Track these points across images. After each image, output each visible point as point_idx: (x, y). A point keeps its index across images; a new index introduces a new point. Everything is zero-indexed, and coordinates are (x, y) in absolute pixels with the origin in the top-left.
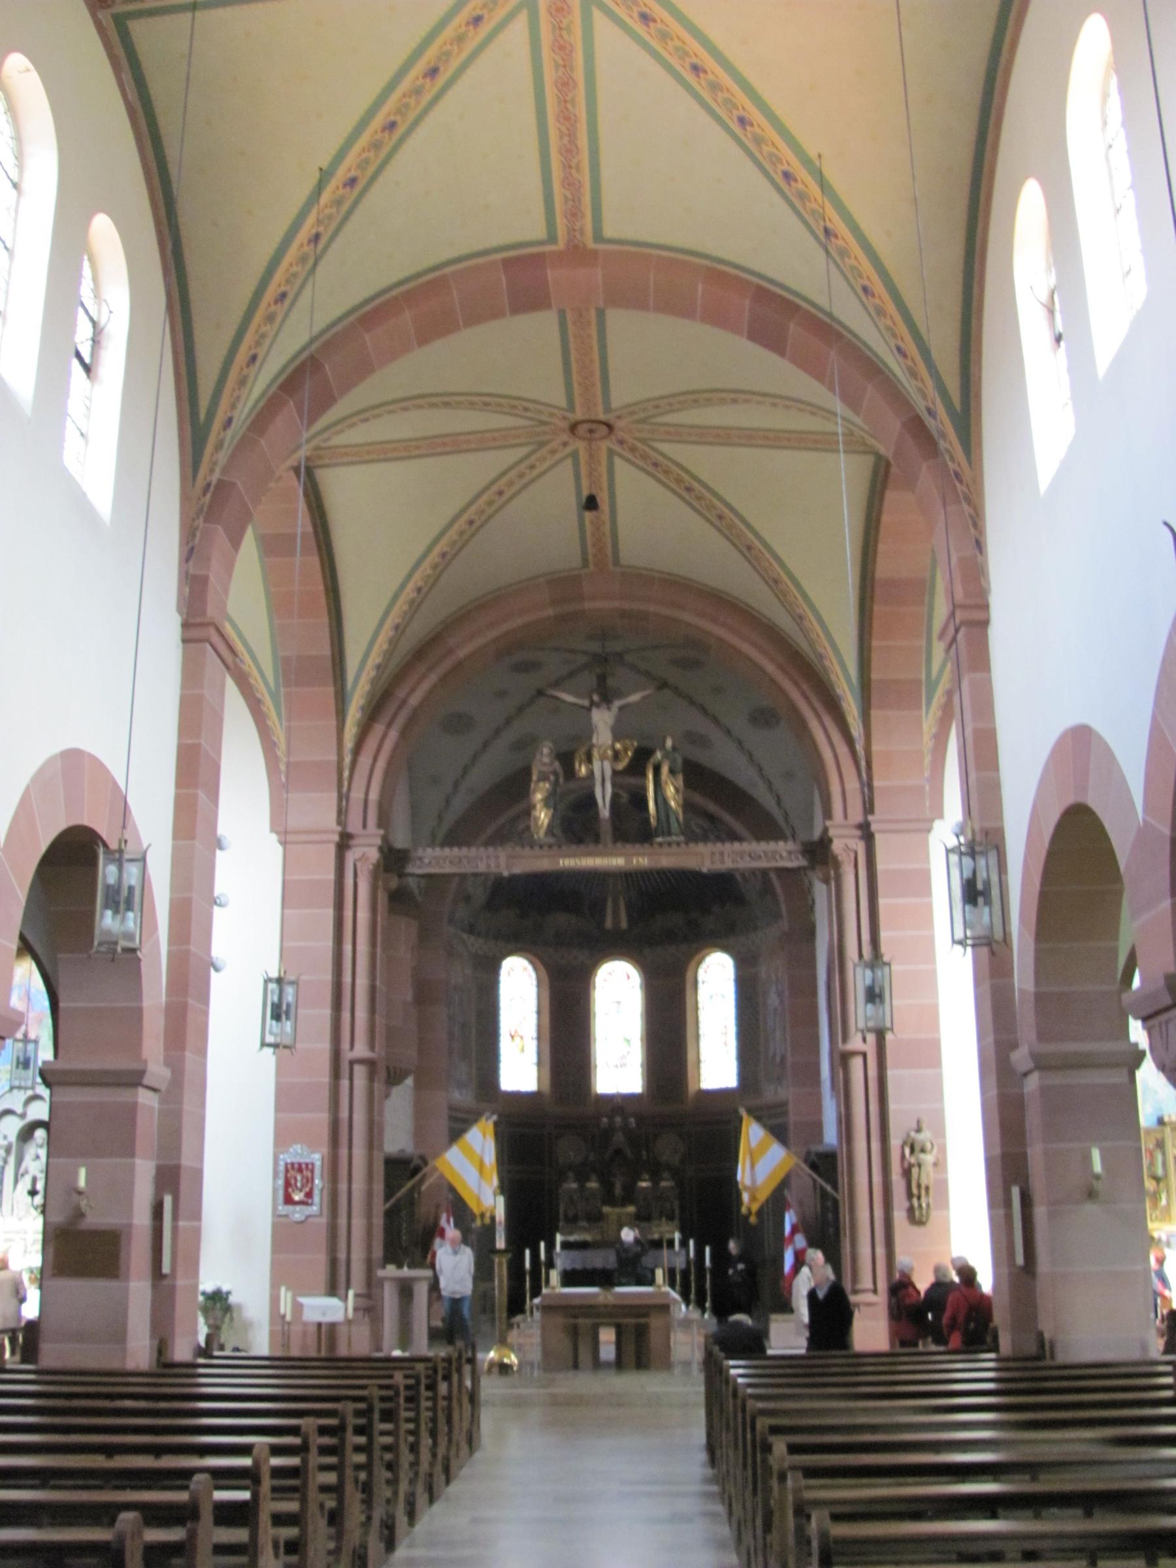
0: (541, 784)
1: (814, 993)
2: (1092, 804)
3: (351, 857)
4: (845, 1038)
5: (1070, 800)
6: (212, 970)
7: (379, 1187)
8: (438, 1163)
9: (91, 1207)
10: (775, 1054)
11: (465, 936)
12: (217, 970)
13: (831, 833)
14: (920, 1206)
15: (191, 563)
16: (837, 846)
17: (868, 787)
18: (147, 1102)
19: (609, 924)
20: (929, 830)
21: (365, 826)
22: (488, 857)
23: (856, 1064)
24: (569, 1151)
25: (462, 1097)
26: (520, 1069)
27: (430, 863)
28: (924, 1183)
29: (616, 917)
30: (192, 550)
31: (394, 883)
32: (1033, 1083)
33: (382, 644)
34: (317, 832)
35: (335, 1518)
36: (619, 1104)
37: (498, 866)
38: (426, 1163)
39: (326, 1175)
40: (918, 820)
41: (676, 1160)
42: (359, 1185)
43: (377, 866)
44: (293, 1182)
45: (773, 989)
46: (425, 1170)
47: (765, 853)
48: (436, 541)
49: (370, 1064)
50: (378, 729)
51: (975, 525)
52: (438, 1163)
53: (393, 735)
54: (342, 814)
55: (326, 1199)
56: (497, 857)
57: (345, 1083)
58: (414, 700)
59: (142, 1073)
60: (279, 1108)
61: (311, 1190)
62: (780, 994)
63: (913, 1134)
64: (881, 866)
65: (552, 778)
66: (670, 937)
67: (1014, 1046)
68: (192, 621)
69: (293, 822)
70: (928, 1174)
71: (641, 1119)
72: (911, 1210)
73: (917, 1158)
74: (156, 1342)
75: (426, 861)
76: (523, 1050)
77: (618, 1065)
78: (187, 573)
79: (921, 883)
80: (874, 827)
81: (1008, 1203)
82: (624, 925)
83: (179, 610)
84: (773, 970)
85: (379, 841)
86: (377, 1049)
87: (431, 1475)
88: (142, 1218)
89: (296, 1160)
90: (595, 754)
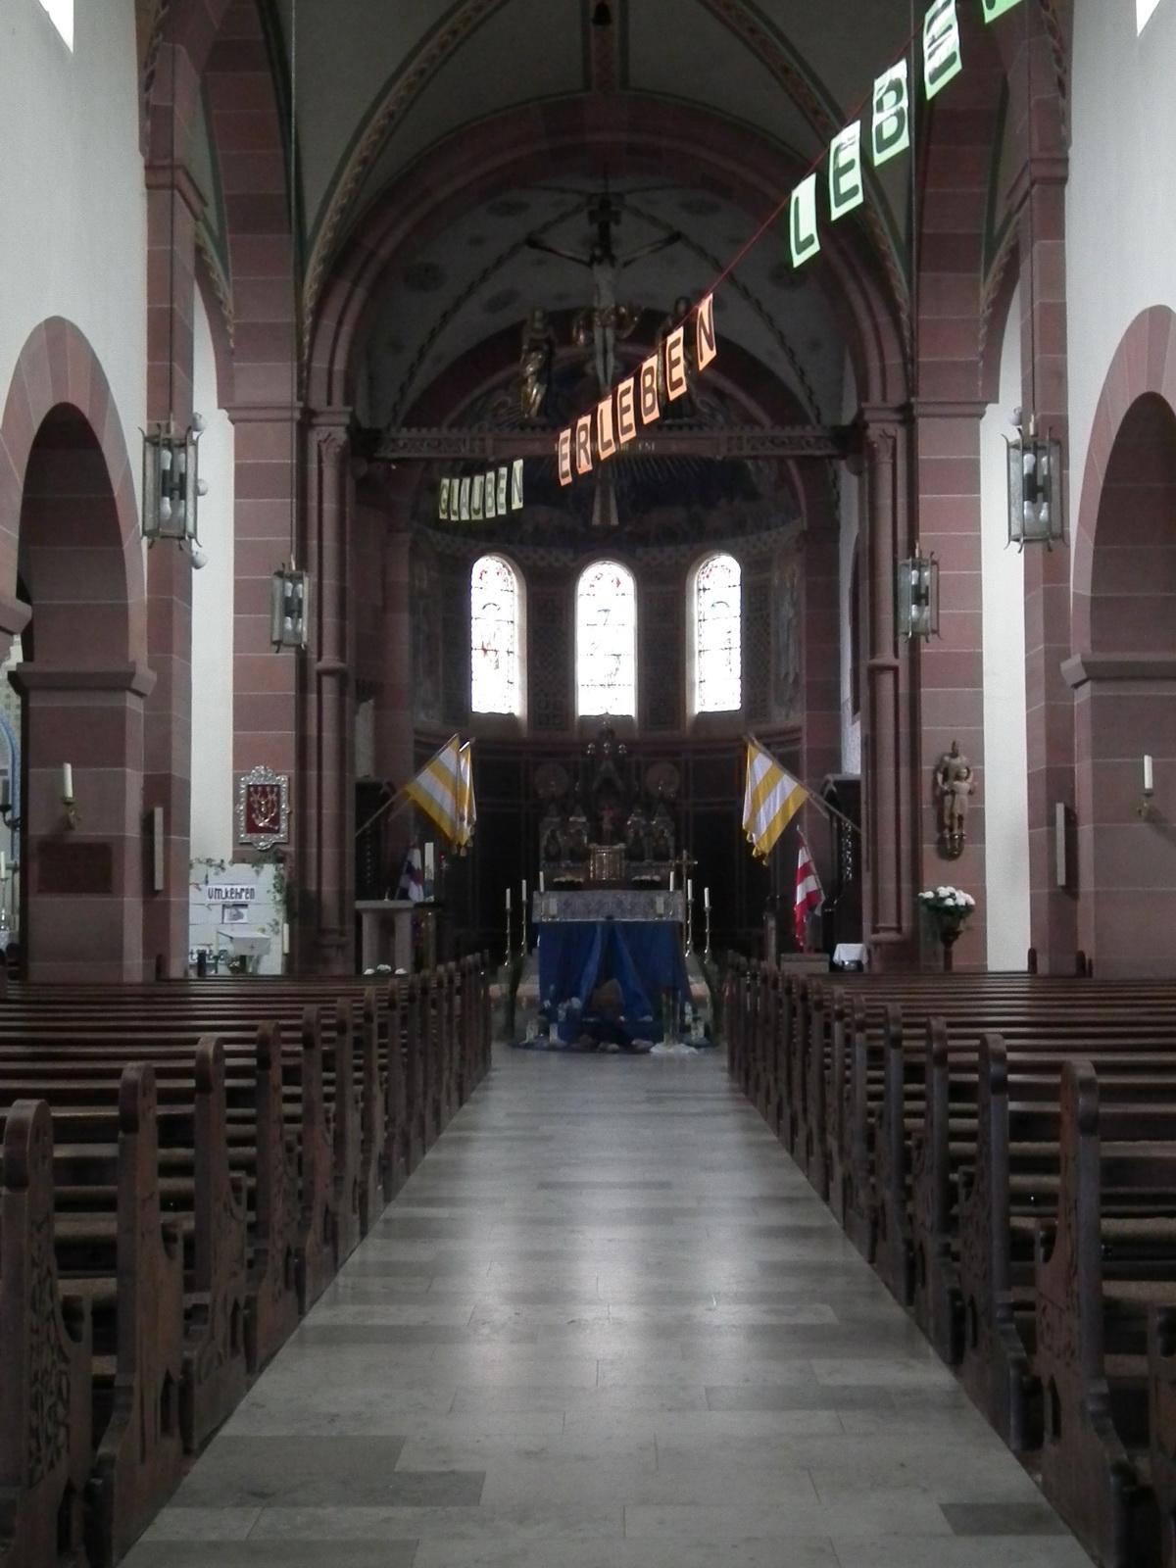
0: (533, 355)
1: (835, 603)
2: (1164, 393)
3: (315, 438)
4: (874, 650)
5: (1143, 389)
6: (193, 570)
7: (351, 813)
8: (410, 788)
9: (79, 819)
10: (787, 674)
11: (430, 532)
12: (197, 567)
13: (867, 416)
14: (952, 837)
15: (151, 90)
16: (873, 432)
17: (909, 360)
18: (133, 707)
19: (596, 520)
20: (981, 416)
21: (329, 403)
22: (473, 439)
23: (887, 679)
24: (551, 783)
25: (427, 719)
26: (497, 686)
27: (405, 445)
28: (957, 811)
29: (605, 513)
30: (151, 76)
31: (363, 469)
32: (1084, 693)
33: (346, 181)
34: (247, 408)
35: (193, 1254)
36: (608, 728)
37: (483, 450)
38: (394, 791)
39: (293, 798)
40: (974, 403)
41: (671, 792)
42: (329, 810)
43: (343, 449)
44: (256, 806)
45: (788, 597)
46: (393, 798)
47: (789, 438)
48: (412, 55)
49: (340, 675)
50: (342, 289)
51: (1059, 61)
52: (410, 788)
53: (360, 294)
54: (303, 386)
55: (293, 823)
56: (482, 440)
57: (313, 697)
58: (384, 253)
59: (131, 675)
60: (238, 725)
61: (278, 815)
62: (794, 604)
63: (947, 758)
64: (924, 455)
65: (546, 347)
66: (669, 535)
67: (1067, 656)
68: (158, 163)
69: (242, 395)
70: (962, 804)
71: (632, 745)
72: (941, 841)
73: (952, 786)
74: (153, 961)
75: (401, 443)
76: (497, 667)
77: (606, 683)
78: (148, 103)
79: (968, 476)
80: (918, 410)
81: (1051, 821)
82: (614, 521)
83: (142, 150)
84: (789, 577)
85: (346, 420)
86: (347, 660)
87: (461, 1076)
88: (133, 831)
89: (261, 781)
90: (597, 321)
